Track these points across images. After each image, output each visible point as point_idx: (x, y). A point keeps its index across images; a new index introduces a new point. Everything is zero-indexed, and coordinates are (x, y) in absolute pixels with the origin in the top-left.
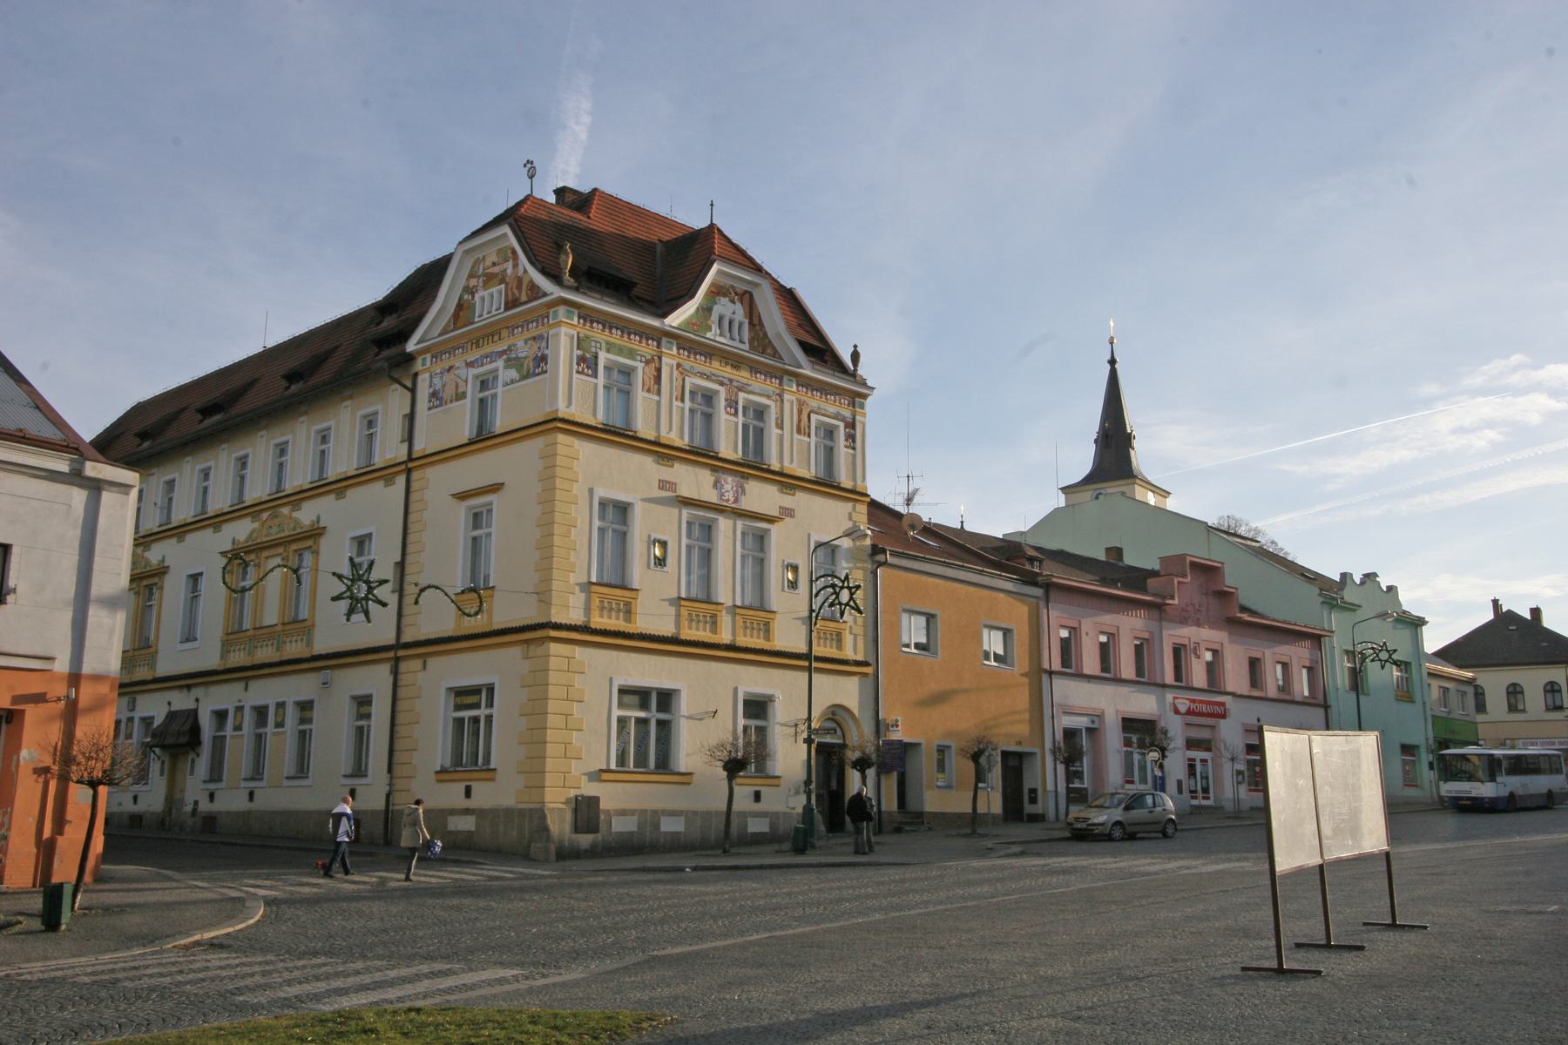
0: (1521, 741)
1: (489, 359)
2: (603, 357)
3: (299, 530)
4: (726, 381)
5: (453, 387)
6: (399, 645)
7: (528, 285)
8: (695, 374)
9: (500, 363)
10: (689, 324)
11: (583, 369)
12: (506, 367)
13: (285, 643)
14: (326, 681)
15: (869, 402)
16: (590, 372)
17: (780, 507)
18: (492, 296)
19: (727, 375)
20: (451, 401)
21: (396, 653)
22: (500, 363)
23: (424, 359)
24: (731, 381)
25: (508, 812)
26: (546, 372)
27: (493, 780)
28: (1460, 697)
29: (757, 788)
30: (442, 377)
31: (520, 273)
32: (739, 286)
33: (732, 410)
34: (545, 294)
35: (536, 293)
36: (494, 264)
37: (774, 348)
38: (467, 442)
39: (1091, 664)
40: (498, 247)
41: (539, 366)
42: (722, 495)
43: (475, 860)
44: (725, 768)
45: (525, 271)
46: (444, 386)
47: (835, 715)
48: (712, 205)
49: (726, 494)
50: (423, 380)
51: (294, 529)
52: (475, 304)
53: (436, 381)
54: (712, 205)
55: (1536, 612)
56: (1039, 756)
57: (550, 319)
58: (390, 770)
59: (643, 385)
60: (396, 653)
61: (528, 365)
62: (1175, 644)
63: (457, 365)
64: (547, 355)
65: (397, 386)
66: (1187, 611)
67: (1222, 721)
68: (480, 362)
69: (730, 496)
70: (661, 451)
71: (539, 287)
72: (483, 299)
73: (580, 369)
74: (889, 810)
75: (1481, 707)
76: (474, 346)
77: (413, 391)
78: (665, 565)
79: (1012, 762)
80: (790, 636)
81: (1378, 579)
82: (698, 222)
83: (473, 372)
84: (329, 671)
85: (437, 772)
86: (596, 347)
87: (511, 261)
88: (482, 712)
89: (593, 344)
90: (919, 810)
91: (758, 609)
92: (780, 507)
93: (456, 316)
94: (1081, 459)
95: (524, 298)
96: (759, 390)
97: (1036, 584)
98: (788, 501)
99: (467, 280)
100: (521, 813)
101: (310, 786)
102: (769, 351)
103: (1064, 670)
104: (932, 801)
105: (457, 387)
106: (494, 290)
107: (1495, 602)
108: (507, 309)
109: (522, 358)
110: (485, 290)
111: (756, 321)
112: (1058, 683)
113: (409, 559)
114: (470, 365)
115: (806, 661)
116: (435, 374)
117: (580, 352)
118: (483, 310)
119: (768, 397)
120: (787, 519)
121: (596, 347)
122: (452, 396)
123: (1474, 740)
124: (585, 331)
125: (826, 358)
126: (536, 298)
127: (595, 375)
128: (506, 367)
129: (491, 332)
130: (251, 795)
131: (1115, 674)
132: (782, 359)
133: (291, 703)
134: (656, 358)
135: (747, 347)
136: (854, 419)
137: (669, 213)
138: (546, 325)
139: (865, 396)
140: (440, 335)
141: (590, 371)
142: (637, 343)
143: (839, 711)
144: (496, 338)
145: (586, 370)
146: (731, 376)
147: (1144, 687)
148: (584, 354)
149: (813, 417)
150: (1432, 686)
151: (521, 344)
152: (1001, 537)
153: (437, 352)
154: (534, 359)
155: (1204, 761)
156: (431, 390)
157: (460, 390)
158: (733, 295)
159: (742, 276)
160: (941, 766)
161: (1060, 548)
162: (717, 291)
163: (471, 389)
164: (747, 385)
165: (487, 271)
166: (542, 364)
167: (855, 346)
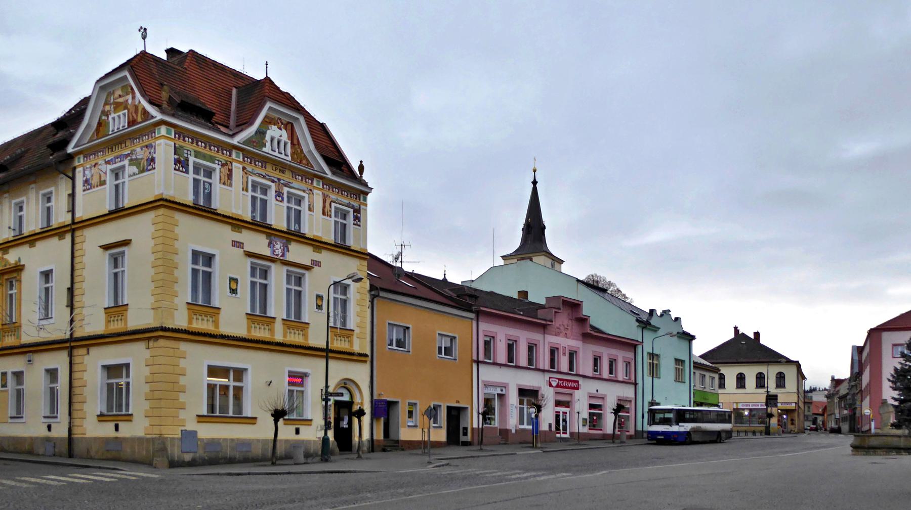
0: (741, 404)
1: (119, 159)
2: (192, 159)
3: (8, 267)
4: (276, 180)
5: (98, 177)
6: (72, 339)
7: (142, 111)
8: (255, 174)
9: (126, 162)
10: (248, 142)
11: (179, 168)
12: (130, 165)
13: (5, 336)
14: (30, 359)
15: (369, 197)
16: (184, 170)
17: (312, 260)
18: (119, 117)
19: (276, 176)
20: (97, 186)
21: (70, 344)
22: (126, 162)
23: (79, 158)
24: (279, 180)
25: (140, 439)
26: (155, 168)
27: (131, 421)
28: (711, 380)
29: (116, 422)
30: (91, 170)
31: (137, 103)
32: (284, 119)
33: (280, 198)
34: (153, 117)
35: (146, 115)
36: (120, 96)
37: (307, 160)
38: (107, 212)
39: (502, 357)
40: (123, 85)
41: (150, 165)
42: (274, 251)
43: (118, 468)
44: (272, 415)
45: (140, 102)
46: (92, 176)
47: (346, 385)
48: (267, 64)
49: (277, 251)
50: (79, 172)
51: (5, 266)
52: (109, 123)
53: (87, 172)
54: (267, 64)
55: (757, 335)
56: (469, 409)
57: (156, 133)
58: (70, 414)
59: (220, 179)
60: (70, 344)
61: (144, 163)
62: (551, 347)
63: (100, 162)
64: (155, 158)
65: (62, 175)
66: (560, 329)
67: (576, 391)
68: (114, 161)
69: (279, 252)
70: (236, 223)
71: (148, 112)
72: (114, 119)
73: (177, 168)
74: (378, 439)
75: (722, 385)
76: (110, 150)
77: (73, 179)
78: (237, 294)
79: (454, 413)
80: (317, 339)
81: (670, 313)
82: (259, 76)
83: (109, 167)
84: (31, 354)
85: (98, 416)
86: (187, 154)
87: (131, 94)
88: (122, 381)
89: (185, 151)
90: (397, 439)
91: (296, 322)
92: (312, 260)
93: (98, 130)
94: (514, 241)
95: (139, 120)
96: (298, 187)
97: (471, 311)
98: (317, 257)
99: (103, 107)
100: (148, 440)
101: (24, 423)
102: (304, 162)
103: (570, 372)
104: (407, 433)
105: (100, 177)
106: (121, 113)
107: (736, 328)
108: (129, 126)
109: (140, 159)
110: (115, 113)
111: (295, 142)
112: (482, 368)
113: (76, 286)
114: (108, 163)
115: (327, 353)
116: (87, 168)
117: (176, 157)
118: (114, 126)
119: (304, 191)
120: (316, 268)
121: (187, 154)
122: (98, 183)
123: (715, 403)
124: (180, 143)
125: (342, 168)
126: (147, 120)
127: (187, 172)
128: (130, 165)
129: (120, 140)
130: (49, 428)
131: (600, 374)
132: (313, 167)
133: (10, 373)
134: (228, 162)
135: (289, 158)
136: (360, 207)
137: (242, 69)
138: (154, 138)
139: (367, 194)
140: (88, 143)
141: (184, 169)
142: (215, 152)
143: (348, 382)
144: (123, 145)
145: (181, 168)
146: (279, 177)
147: (628, 385)
148: (179, 158)
149: (333, 205)
150: (696, 374)
151: (138, 150)
152: (460, 284)
153: (86, 153)
154: (147, 160)
155: (565, 413)
156: (85, 179)
157: (103, 179)
158: (280, 124)
159: (287, 112)
160: (410, 414)
161: (491, 290)
162: (268, 121)
163: (109, 178)
164: (290, 183)
165: (116, 101)
166: (152, 163)
167: (361, 162)
